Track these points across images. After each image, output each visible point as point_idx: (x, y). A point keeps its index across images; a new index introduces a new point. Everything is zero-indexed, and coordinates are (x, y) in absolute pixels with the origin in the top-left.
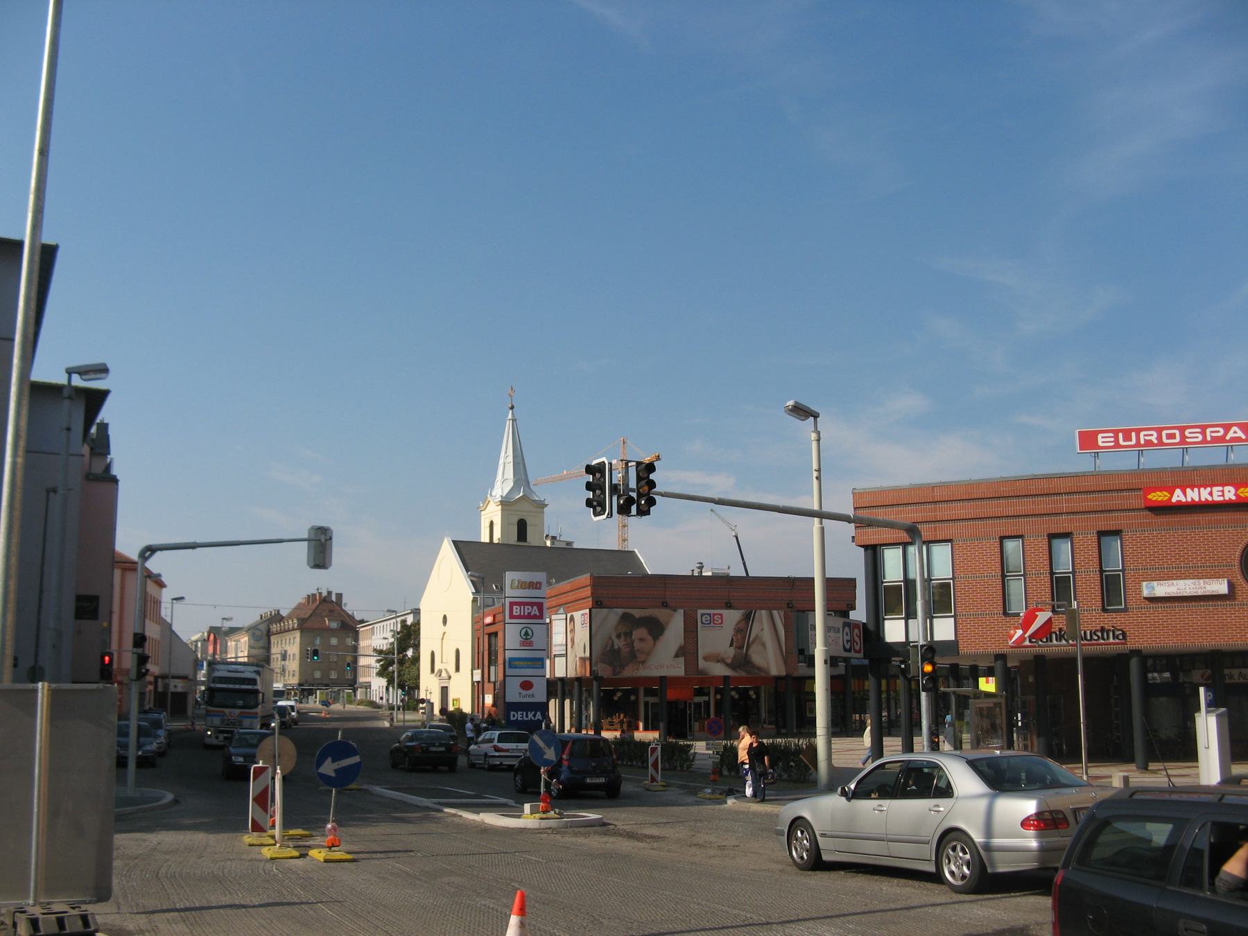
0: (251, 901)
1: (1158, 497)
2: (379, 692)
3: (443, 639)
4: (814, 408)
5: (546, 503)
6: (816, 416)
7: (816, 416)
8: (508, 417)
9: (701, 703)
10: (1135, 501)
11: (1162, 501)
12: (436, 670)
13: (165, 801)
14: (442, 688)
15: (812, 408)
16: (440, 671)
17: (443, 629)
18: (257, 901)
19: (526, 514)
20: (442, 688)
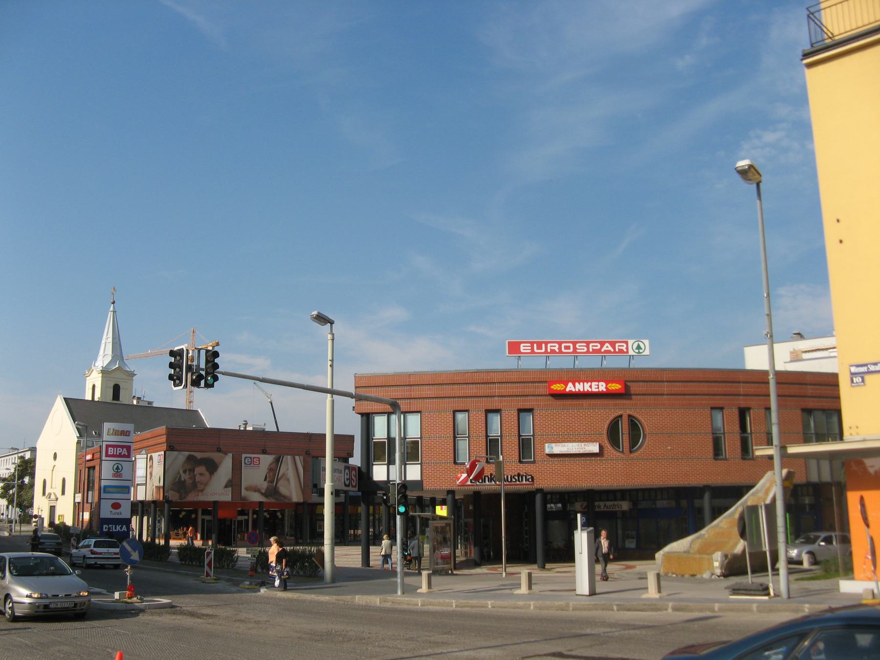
6: (332, 323)
7: (332, 323)
10: (542, 389)
11: (560, 390)
14: (51, 507)
20: (51, 507)
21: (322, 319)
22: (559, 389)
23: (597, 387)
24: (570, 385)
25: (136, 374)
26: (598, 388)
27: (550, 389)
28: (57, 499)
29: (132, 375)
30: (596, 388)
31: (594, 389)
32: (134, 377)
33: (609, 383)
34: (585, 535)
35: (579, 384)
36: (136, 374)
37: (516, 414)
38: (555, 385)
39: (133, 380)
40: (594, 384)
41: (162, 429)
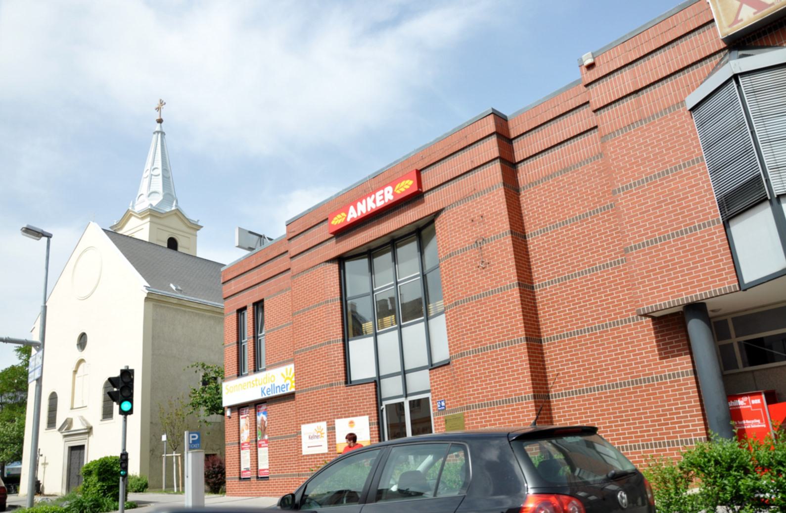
0: (450, 460)
1: (338, 221)
2: (610, 94)
3: (75, 372)
4: (47, 230)
5: (199, 224)
6: (49, 236)
7: (49, 236)
8: (134, 194)
9: (386, 301)
10: (323, 232)
11: (341, 223)
12: (59, 422)
13: (265, 418)
14: (72, 449)
15: (428, 142)
16: (68, 423)
17: (78, 354)
18: (450, 460)
19: (178, 232)
20: (72, 449)
21: (32, 232)
22: (339, 222)
23: (382, 197)
24: (352, 208)
25: (202, 227)
26: (384, 199)
27: (331, 226)
28: (89, 431)
29: (197, 227)
30: (381, 201)
31: (380, 204)
32: (198, 232)
33: (397, 184)
34: (190, 455)
35: (361, 203)
36: (202, 227)
37: (235, 315)
38: (335, 218)
39: (196, 236)
40: (370, 200)
41: (589, 53)
